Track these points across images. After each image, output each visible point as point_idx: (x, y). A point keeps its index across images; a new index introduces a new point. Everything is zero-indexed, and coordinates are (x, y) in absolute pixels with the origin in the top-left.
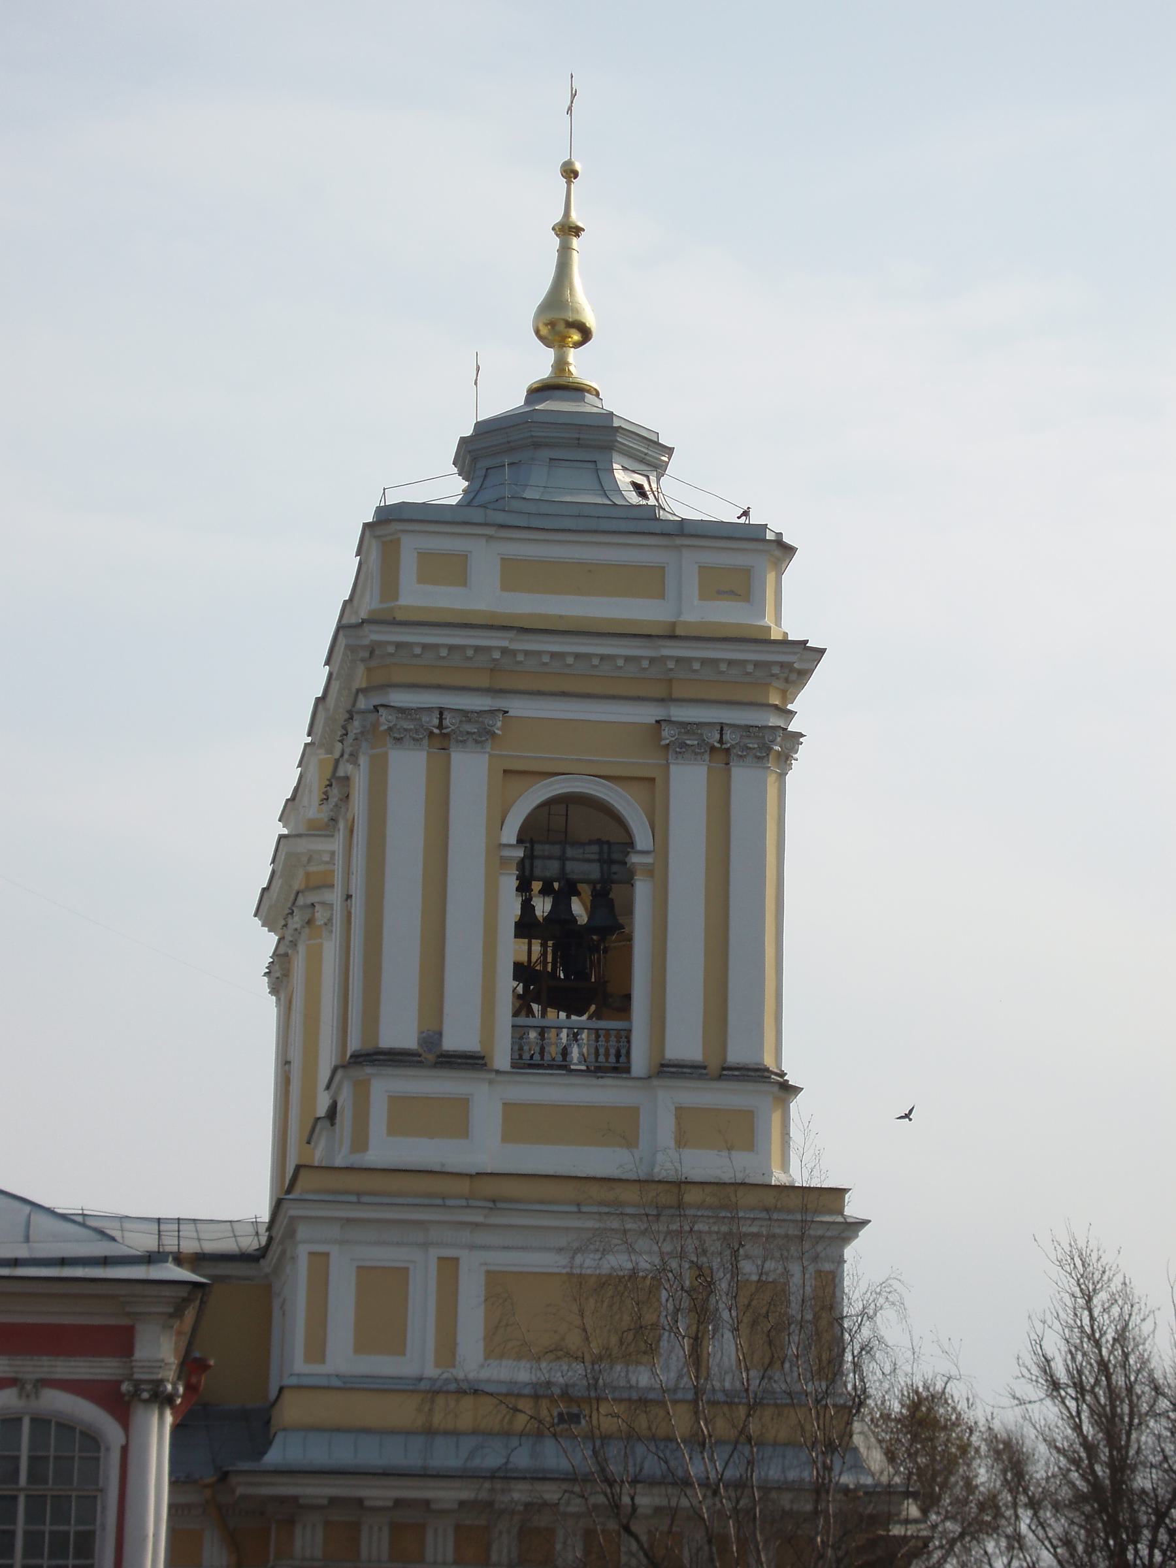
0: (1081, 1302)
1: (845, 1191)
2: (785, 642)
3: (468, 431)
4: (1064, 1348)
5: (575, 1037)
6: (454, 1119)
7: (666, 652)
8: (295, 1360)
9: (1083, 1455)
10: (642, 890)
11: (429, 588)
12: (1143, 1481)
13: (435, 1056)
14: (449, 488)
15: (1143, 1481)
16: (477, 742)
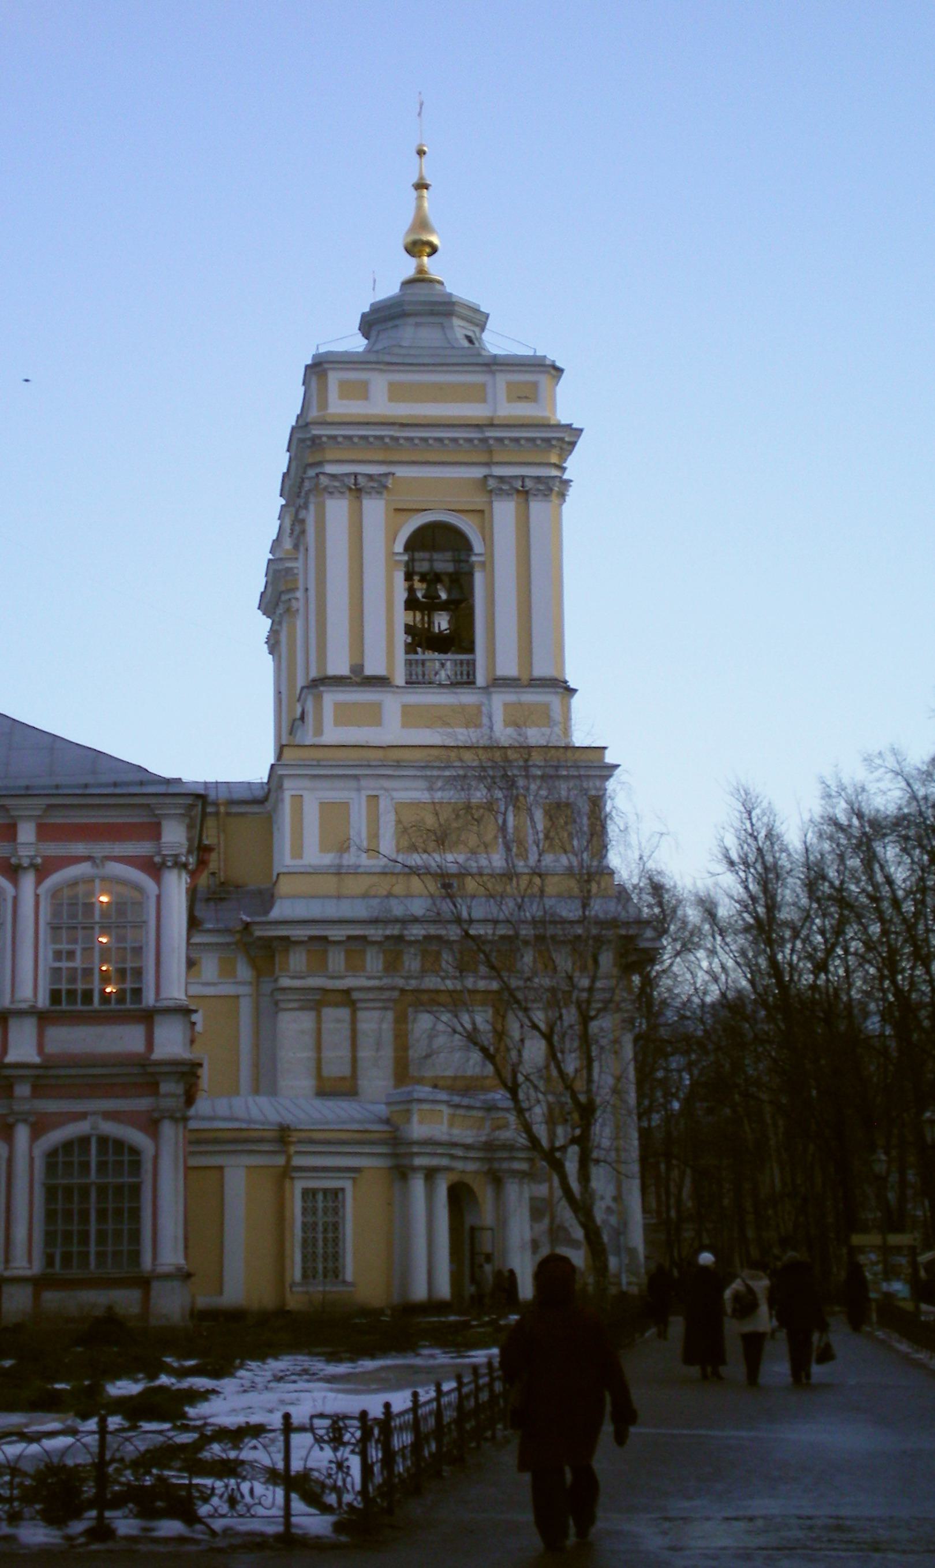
0: (745, 815)
1: (605, 748)
2: (559, 426)
3: (367, 309)
4: (736, 841)
5: (443, 665)
6: (374, 716)
7: (488, 434)
8: (285, 859)
9: (750, 902)
10: (479, 578)
11: (345, 402)
12: (784, 915)
13: (361, 679)
14: (358, 344)
15: (784, 915)
16: (378, 493)
